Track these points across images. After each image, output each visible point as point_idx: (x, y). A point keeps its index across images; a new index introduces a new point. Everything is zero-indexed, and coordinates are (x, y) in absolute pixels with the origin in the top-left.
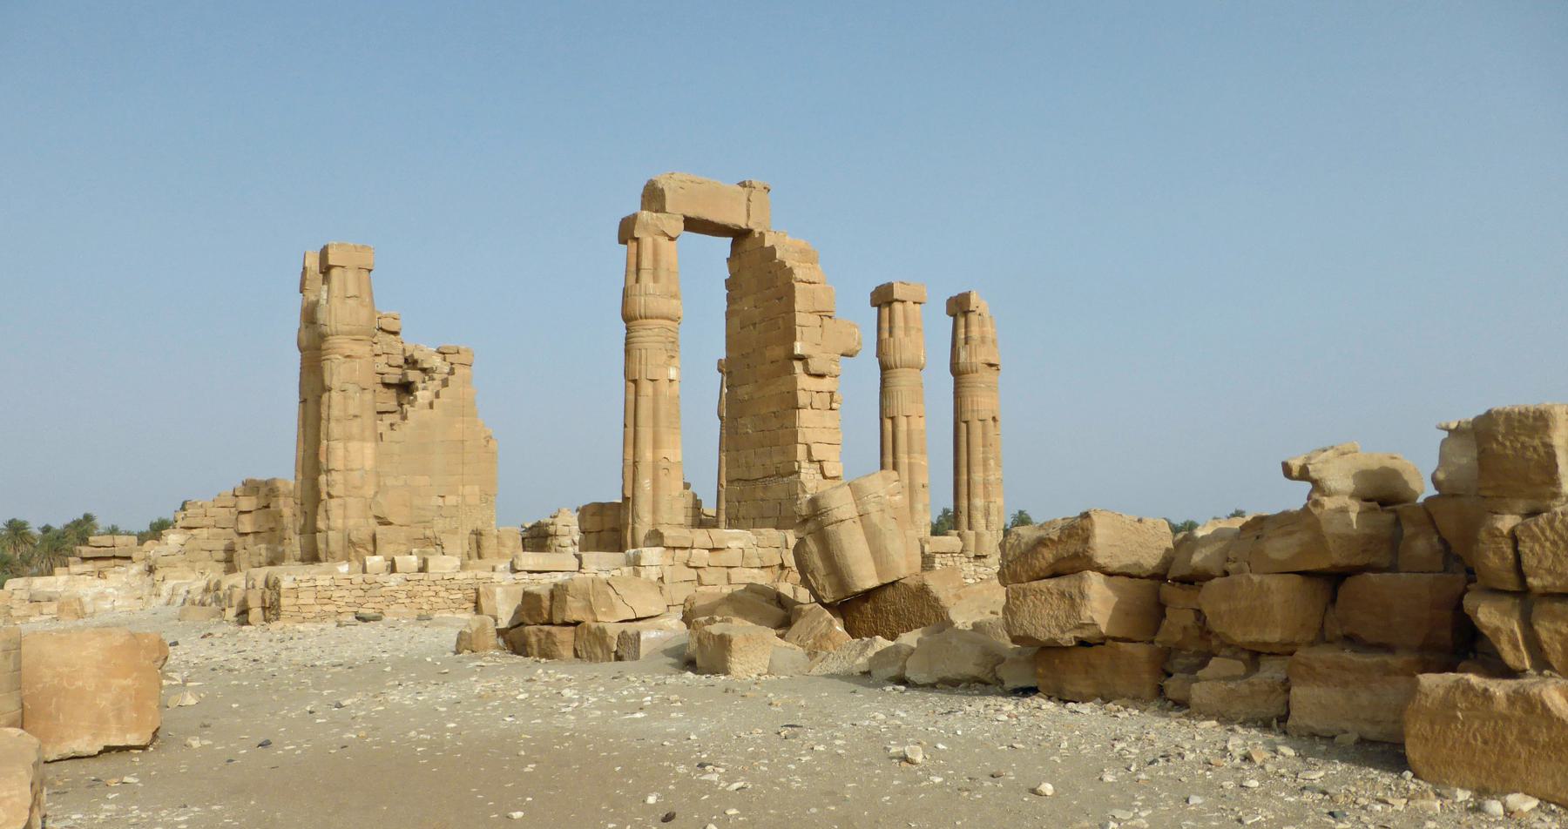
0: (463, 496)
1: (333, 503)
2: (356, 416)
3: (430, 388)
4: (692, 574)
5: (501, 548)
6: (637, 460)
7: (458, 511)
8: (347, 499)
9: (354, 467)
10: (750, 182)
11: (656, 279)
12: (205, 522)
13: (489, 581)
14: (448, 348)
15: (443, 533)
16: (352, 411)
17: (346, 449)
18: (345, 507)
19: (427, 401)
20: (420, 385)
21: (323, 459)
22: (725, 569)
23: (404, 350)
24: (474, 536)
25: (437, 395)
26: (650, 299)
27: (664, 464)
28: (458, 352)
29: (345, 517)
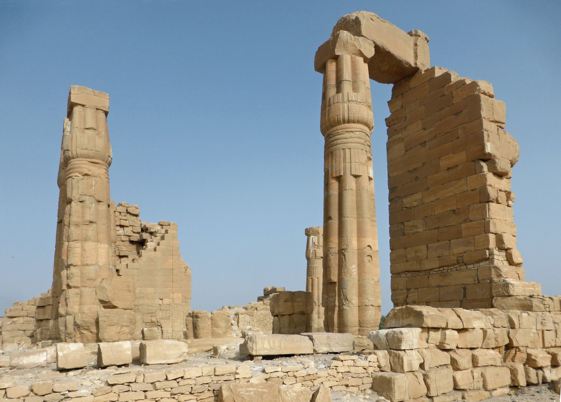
0: (173, 299)
1: (71, 292)
2: (91, 222)
3: (154, 241)
4: (445, 358)
5: (215, 329)
6: (344, 247)
7: (170, 307)
8: (83, 289)
9: (89, 263)
10: (416, 31)
11: (355, 89)
12: (22, 313)
13: (233, 378)
14: (164, 222)
15: (162, 319)
16: (88, 218)
17: (83, 249)
18: (81, 295)
19: (153, 248)
20: (149, 240)
21: (64, 258)
22: (469, 350)
23: (141, 224)
24: (191, 319)
25: (158, 244)
26: (353, 105)
27: (368, 251)
28: (169, 225)
29: (81, 304)
